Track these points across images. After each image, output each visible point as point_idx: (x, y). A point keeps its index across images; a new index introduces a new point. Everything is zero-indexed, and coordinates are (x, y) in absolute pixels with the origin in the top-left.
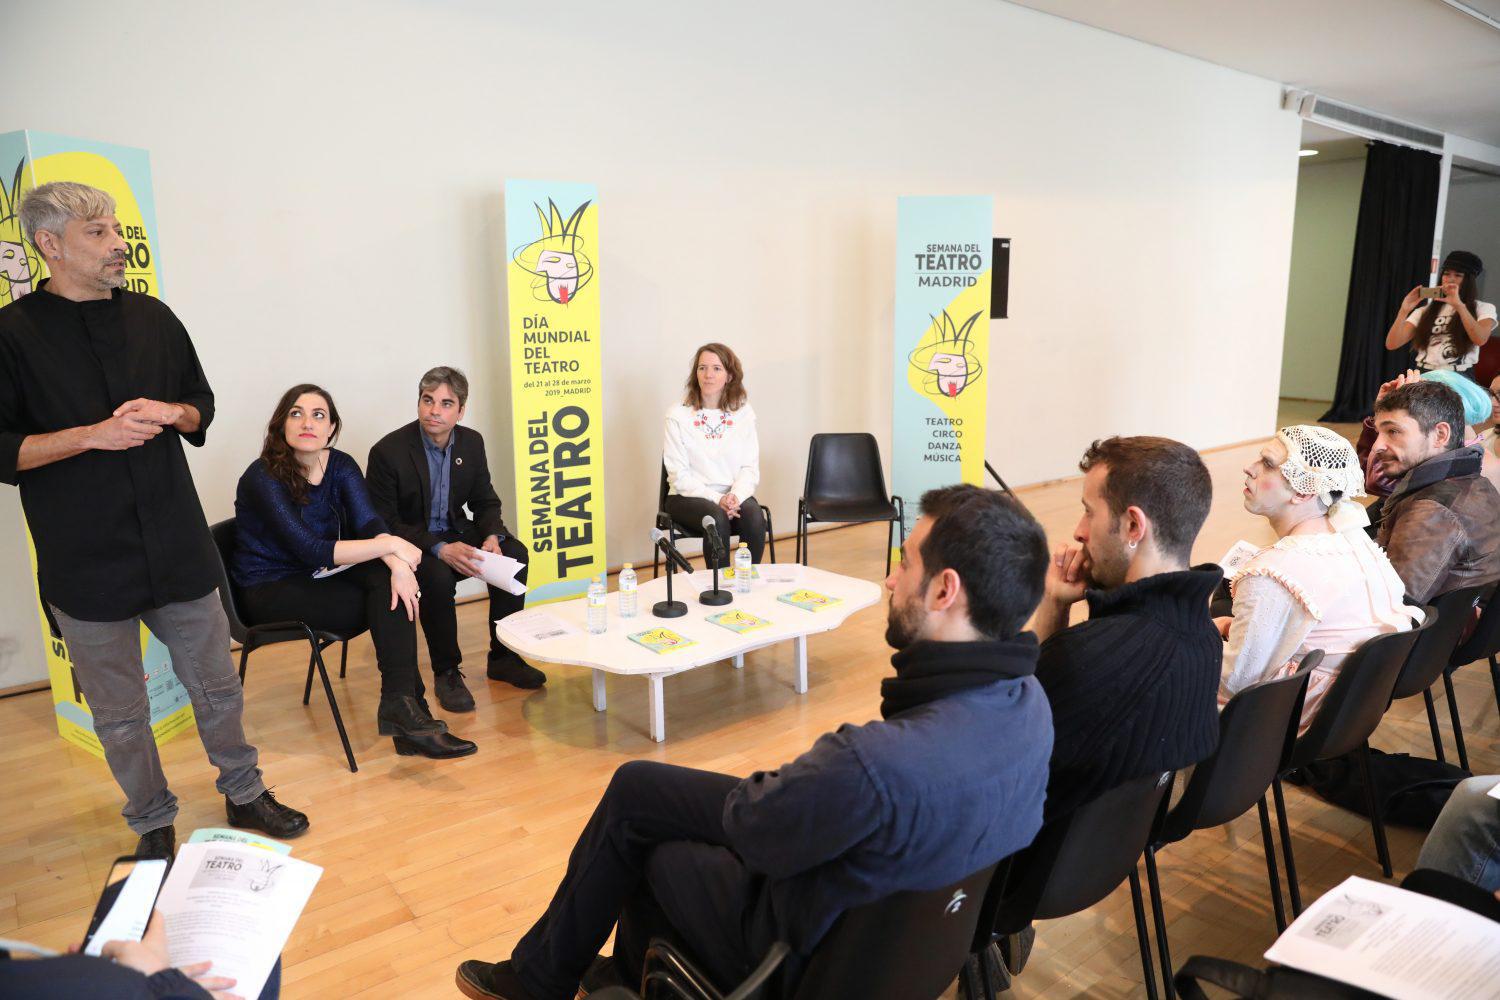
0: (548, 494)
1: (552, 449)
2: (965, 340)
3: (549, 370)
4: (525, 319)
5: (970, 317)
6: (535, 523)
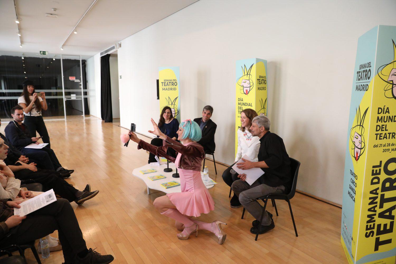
0: (376, 206)
1: (381, 182)
2: (174, 104)
3: (386, 138)
4: (379, 108)
5: (175, 98)
6: (368, 222)
